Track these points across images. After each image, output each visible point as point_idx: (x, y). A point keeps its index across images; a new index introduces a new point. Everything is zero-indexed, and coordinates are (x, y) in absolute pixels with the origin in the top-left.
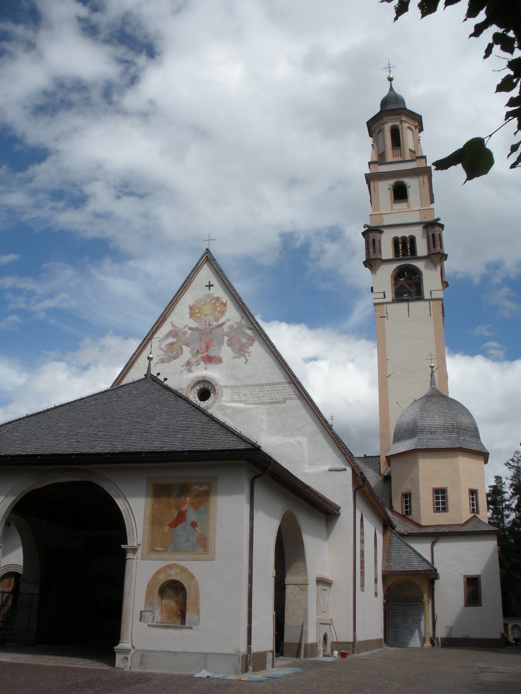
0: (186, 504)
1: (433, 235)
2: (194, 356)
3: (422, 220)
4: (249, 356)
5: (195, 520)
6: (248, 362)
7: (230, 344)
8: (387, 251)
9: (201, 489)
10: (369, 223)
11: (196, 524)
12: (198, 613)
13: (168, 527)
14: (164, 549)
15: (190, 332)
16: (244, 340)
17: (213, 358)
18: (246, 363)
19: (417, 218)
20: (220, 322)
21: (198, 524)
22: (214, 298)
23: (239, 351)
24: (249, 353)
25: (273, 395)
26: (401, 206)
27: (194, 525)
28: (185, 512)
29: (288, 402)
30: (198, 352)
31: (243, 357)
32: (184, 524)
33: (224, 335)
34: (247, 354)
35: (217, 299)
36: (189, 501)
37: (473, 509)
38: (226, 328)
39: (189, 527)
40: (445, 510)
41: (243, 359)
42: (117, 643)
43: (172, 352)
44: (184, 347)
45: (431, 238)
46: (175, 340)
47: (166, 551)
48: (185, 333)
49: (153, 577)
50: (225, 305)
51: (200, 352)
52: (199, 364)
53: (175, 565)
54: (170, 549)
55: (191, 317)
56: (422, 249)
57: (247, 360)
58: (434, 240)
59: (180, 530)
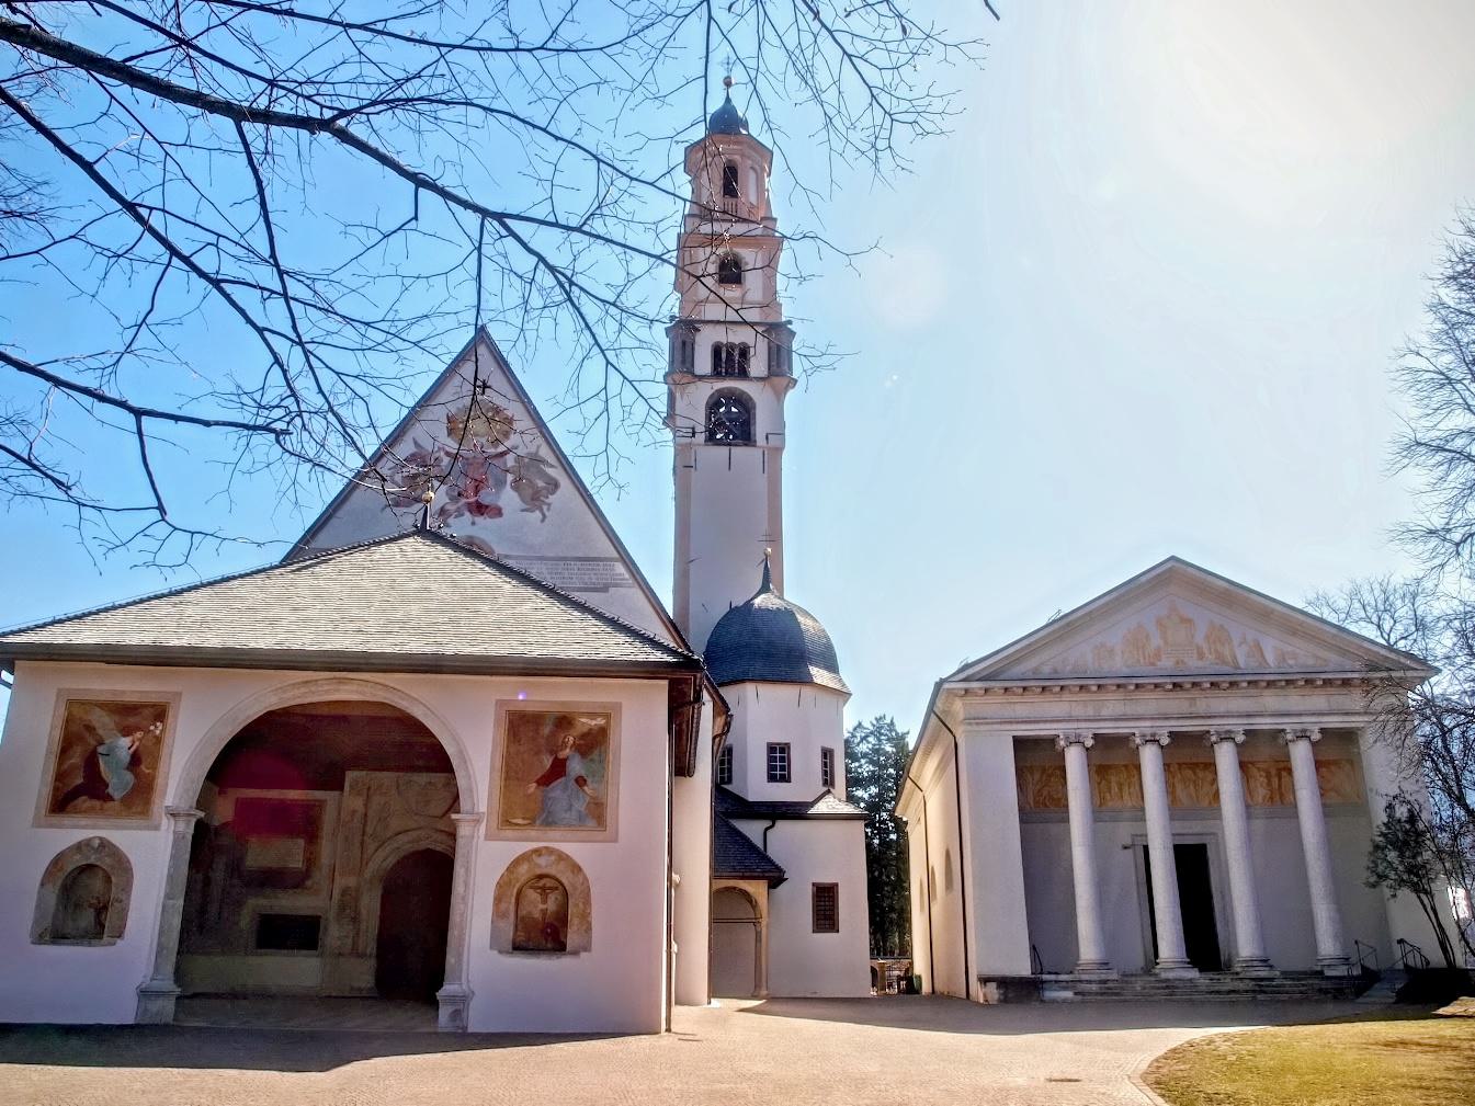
1: (779, 347)
2: (453, 499)
3: (764, 321)
4: (548, 509)
5: (583, 773)
6: (546, 520)
7: (516, 486)
8: (703, 363)
9: (593, 723)
11: (585, 781)
13: (535, 785)
14: (526, 822)
17: (487, 507)
18: (543, 521)
20: (501, 449)
21: (589, 781)
23: (533, 499)
25: (587, 577)
27: (581, 781)
28: (565, 760)
29: (612, 590)
30: (459, 495)
31: (537, 512)
34: (545, 508)
37: (826, 780)
38: (510, 460)
39: (572, 783)
40: (786, 779)
41: (538, 514)
42: (440, 986)
47: (532, 823)
52: (462, 515)
53: (546, 848)
54: (538, 822)
55: (449, 435)
56: (757, 366)
57: (544, 516)
59: (557, 790)
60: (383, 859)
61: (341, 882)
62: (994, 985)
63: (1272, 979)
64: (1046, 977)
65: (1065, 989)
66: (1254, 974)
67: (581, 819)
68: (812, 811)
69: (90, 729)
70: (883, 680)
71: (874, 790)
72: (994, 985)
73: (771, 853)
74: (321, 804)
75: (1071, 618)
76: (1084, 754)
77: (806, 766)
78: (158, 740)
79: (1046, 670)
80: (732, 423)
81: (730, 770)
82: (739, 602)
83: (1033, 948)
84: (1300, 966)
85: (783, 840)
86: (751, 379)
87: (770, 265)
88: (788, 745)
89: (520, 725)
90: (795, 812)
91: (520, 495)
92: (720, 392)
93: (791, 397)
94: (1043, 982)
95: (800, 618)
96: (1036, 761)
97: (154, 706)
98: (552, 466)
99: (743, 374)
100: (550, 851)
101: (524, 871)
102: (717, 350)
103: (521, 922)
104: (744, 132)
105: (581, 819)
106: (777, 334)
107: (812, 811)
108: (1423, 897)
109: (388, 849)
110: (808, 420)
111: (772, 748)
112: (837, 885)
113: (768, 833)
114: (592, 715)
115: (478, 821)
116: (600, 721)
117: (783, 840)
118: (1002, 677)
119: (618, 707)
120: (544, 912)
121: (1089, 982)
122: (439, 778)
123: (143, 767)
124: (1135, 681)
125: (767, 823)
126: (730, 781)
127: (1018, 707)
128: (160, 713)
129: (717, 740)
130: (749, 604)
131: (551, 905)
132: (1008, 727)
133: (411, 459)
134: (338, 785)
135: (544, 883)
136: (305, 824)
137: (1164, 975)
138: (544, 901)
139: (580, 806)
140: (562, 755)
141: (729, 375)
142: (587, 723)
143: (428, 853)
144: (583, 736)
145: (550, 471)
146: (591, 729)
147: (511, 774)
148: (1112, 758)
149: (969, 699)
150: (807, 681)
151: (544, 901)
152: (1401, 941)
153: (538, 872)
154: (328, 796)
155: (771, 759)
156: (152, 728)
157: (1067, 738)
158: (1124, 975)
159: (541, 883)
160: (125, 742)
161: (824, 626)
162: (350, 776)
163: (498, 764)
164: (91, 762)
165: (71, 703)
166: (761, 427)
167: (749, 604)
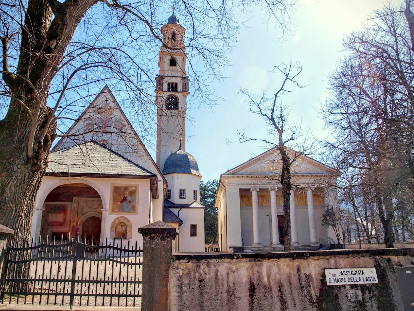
1: (185, 83)
8: (165, 87)
9: (133, 189)
10: (158, 74)
12: (132, 234)
15: (97, 119)
27: (130, 202)
33: (113, 122)
39: (128, 203)
40: (184, 198)
45: (184, 84)
46: (90, 122)
47: (119, 211)
51: (349, 164)
54: (121, 211)
56: (180, 88)
59: (124, 204)
60: (82, 219)
62: (232, 249)
63: (299, 247)
64: (244, 247)
65: (249, 249)
66: (295, 246)
67: (130, 209)
68: (191, 206)
70: (209, 172)
71: (212, 199)
72: (232, 249)
73: (180, 217)
74: (67, 206)
75: (255, 159)
76: (257, 192)
77: (189, 196)
79: (248, 172)
80: (173, 104)
81: (170, 196)
82: (173, 152)
83: (242, 240)
84: (307, 244)
85: (183, 213)
87: (184, 60)
88: (185, 189)
89: (116, 189)
90: (187, 206)
92: (169, 96)
93: (188, 98)
94: (244, 248)
95: (189, 157)
96: (245, 194)
98: (124, 121)
99: (176, 90)
100: (123, 217)
101: (117, 222)
102: (169, 84)
103: (116, 233)
104: (178, 23)
105: (130, 209)
106: (185, 79)
107: (191, 206)
108: (334, 227)
109: (84, 216)
110: (191, 103)
111: (181, 190)
112: (196, 225)
113: (180, 211)
114: (132, 187)
115: (107, 211)
116: (134, 188)
117: (183, 213)
118: (237, 173)
119: (139, 185)
120: (122, 230)
121: (256, 248)
122: (96, 199)
124: (270, 175)
125: (180, 209)
126: (170, 198)
127: (241, 181)
129: (165, 190)
130: (176, 153)
131: (124, 229)
132: (238, 186)
135: (122, 224)
136: (63, 210)
137: (273, 246)
139: (130, 207)
140: (126, 196)
141: (172, 91)
142: (131, 189)
143: (93, 218)
144: (130, 192)
145: (123, 122)
147: (114, 200)
148: (263, 194)
149: (229, 179)
150: (190, 173)
151: (122, 228)
152: (329, 238)
153: (120, 222)
155: (181, 193)
157: (252, 189)
158: (264, 246)
161: (195, 159)
162: (74, 198)
163: (111, 198)
166: (180, 106)
167: (176, 153)
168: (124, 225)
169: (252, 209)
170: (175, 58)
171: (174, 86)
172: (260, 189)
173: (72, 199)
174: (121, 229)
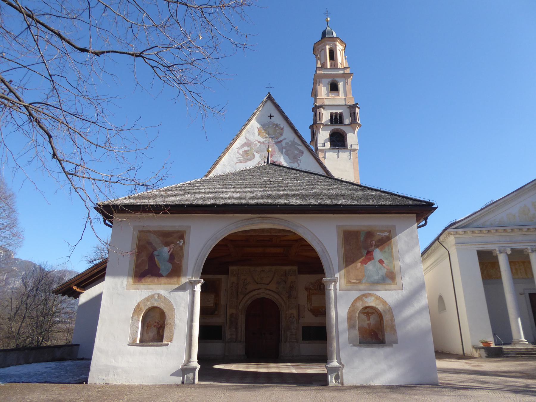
0: (372, 246)
9: (383, 234)
16: (296, 152)
19: (342, 102)
20: (279, 140)
22: (274, 124)
24: (300, 160)
26: (332, 95)
32: (373, 261)
34: (299, 161)
35: (277, 125)
36: (374, 244)
39: (378, 264)
43: (247, 156)
44: (255, 153)
46: (249, 148)
48: (256, 145)
49: (352, 304)
50: (282, 129)
53: (369, 293)
56: (347, 121)
58: (353, 116)
61: (230, 311)
69: (150, 244)
76: (507, 256)
78: (182, 248)
86: (345, 125)
91: (289, 157)
97: (178, 232)
98: (300, 145)
109: (247, 297)
114: (383, 231)
116: (386, 234)
120: (369, 325)
123: (175, 261)
128: (181, 236)
133: (245, 144)
134: (226, 272)
138: (369, 319)
141: (336, 122)
146: (382, 238)
151: (369, 319)
154: (223, 277)
156: (178, 242)
159: (366, 311)
160: (166, 249)
162: (231, 268)
164: (151, 259)
165: (140, 232)
168: (372, 313)
169: (501, 283)
170: (336, 81)
171: (338, 118)
172: (512, 250)
173: (228, 269)
174: (367, 322)
